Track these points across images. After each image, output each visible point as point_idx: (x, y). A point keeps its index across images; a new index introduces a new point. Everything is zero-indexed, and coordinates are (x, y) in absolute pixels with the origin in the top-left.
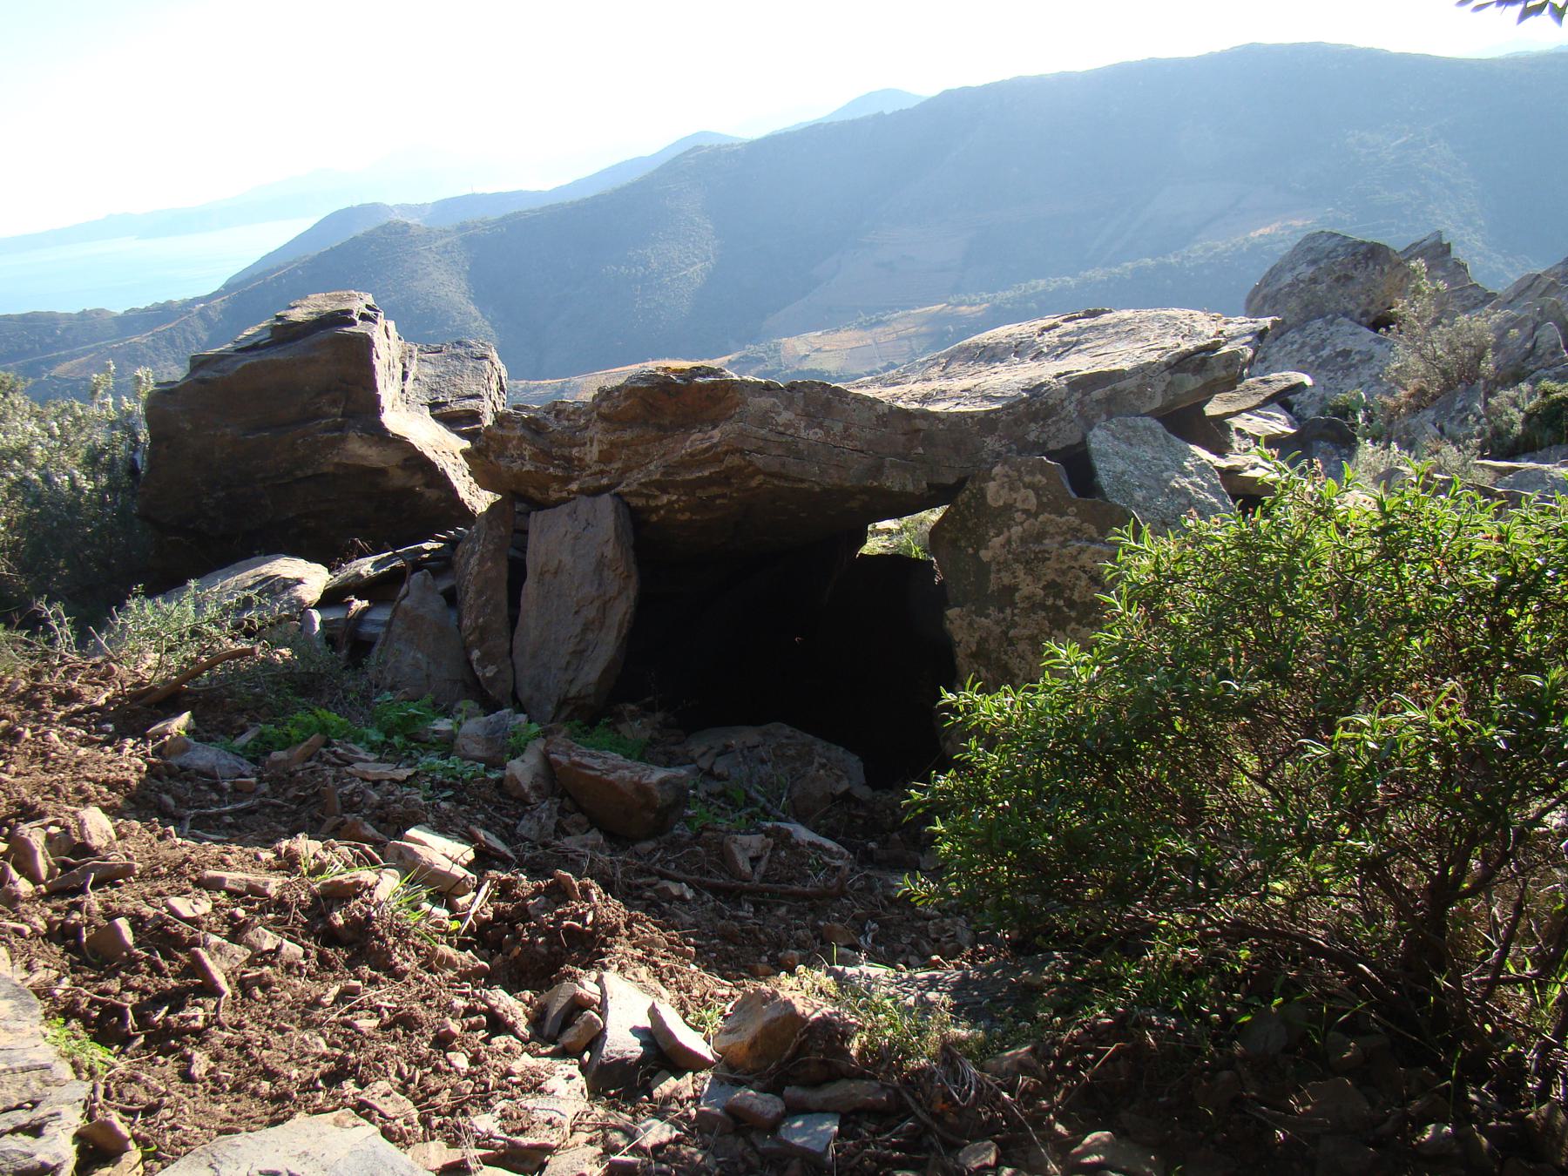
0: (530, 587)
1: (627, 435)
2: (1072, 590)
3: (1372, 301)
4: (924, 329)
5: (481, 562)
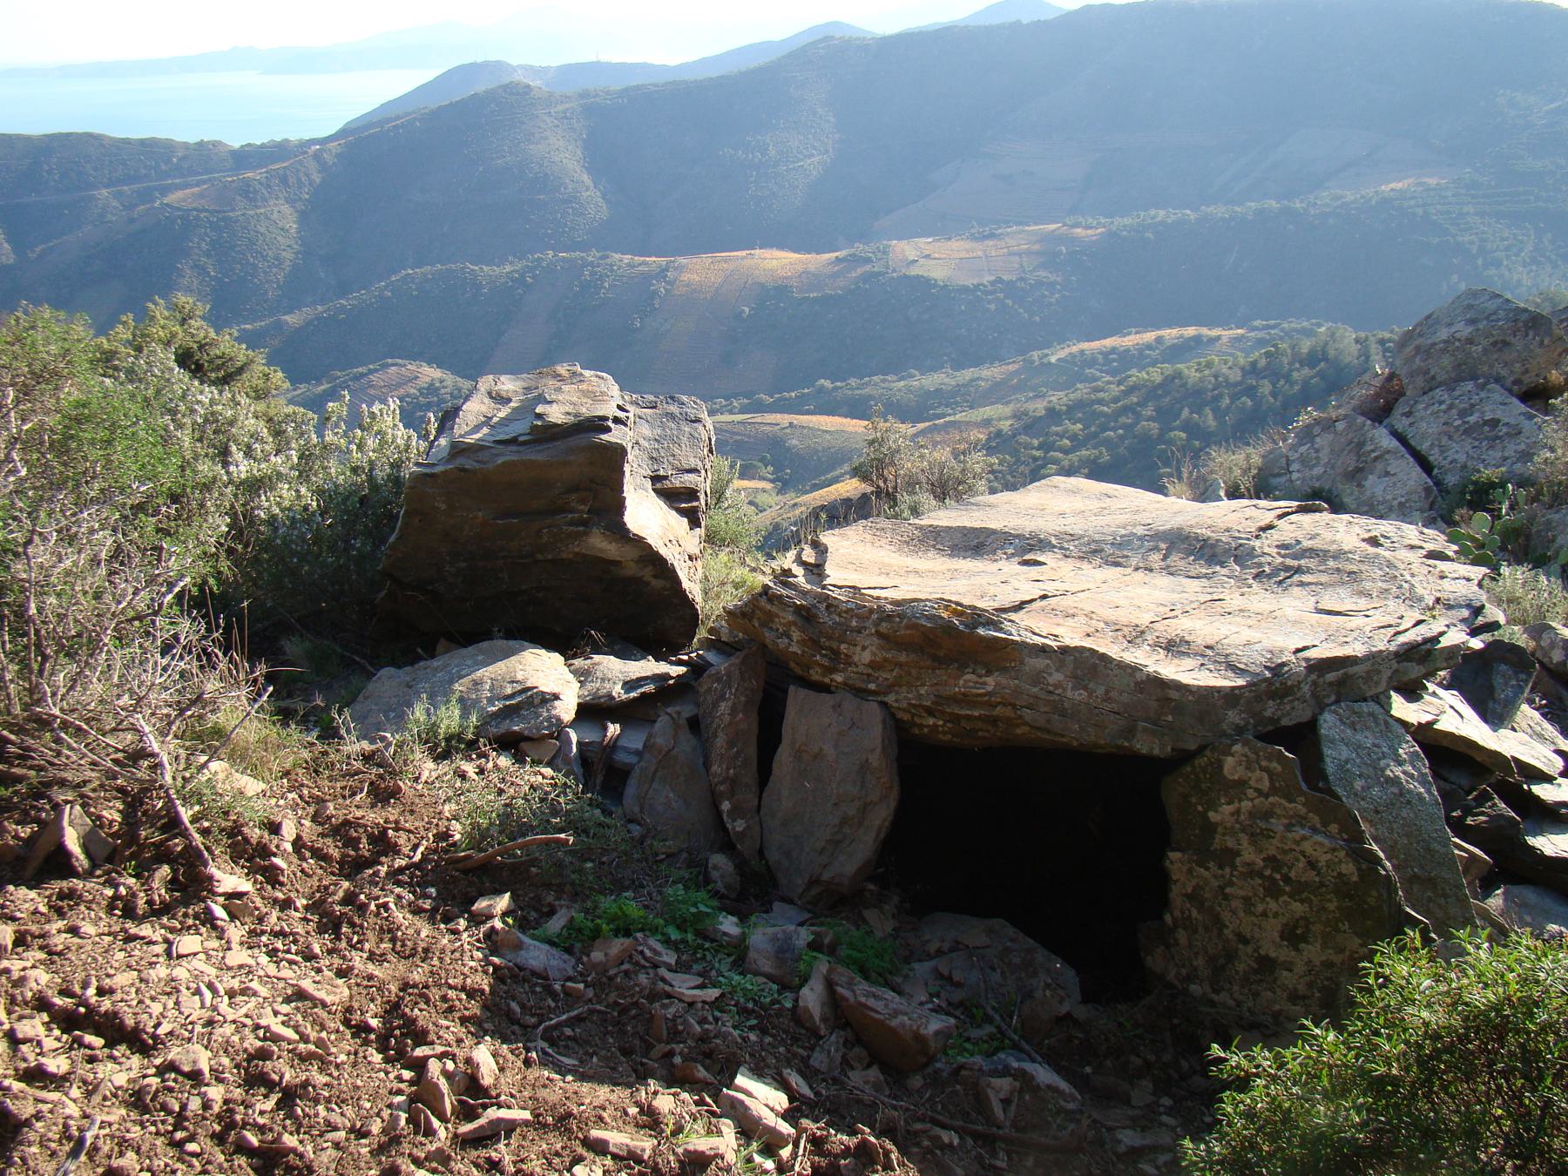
0: (783, 757)
1: (903, 658)
2: (1290, 868)
3: (1527, 371)
4: (1036, 247)
5: (734, 711)
